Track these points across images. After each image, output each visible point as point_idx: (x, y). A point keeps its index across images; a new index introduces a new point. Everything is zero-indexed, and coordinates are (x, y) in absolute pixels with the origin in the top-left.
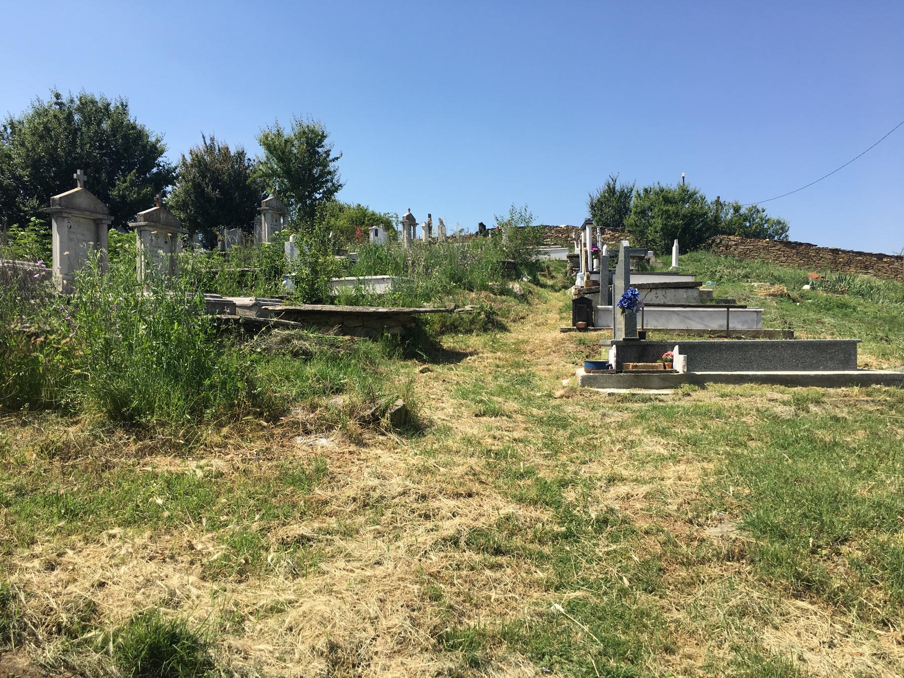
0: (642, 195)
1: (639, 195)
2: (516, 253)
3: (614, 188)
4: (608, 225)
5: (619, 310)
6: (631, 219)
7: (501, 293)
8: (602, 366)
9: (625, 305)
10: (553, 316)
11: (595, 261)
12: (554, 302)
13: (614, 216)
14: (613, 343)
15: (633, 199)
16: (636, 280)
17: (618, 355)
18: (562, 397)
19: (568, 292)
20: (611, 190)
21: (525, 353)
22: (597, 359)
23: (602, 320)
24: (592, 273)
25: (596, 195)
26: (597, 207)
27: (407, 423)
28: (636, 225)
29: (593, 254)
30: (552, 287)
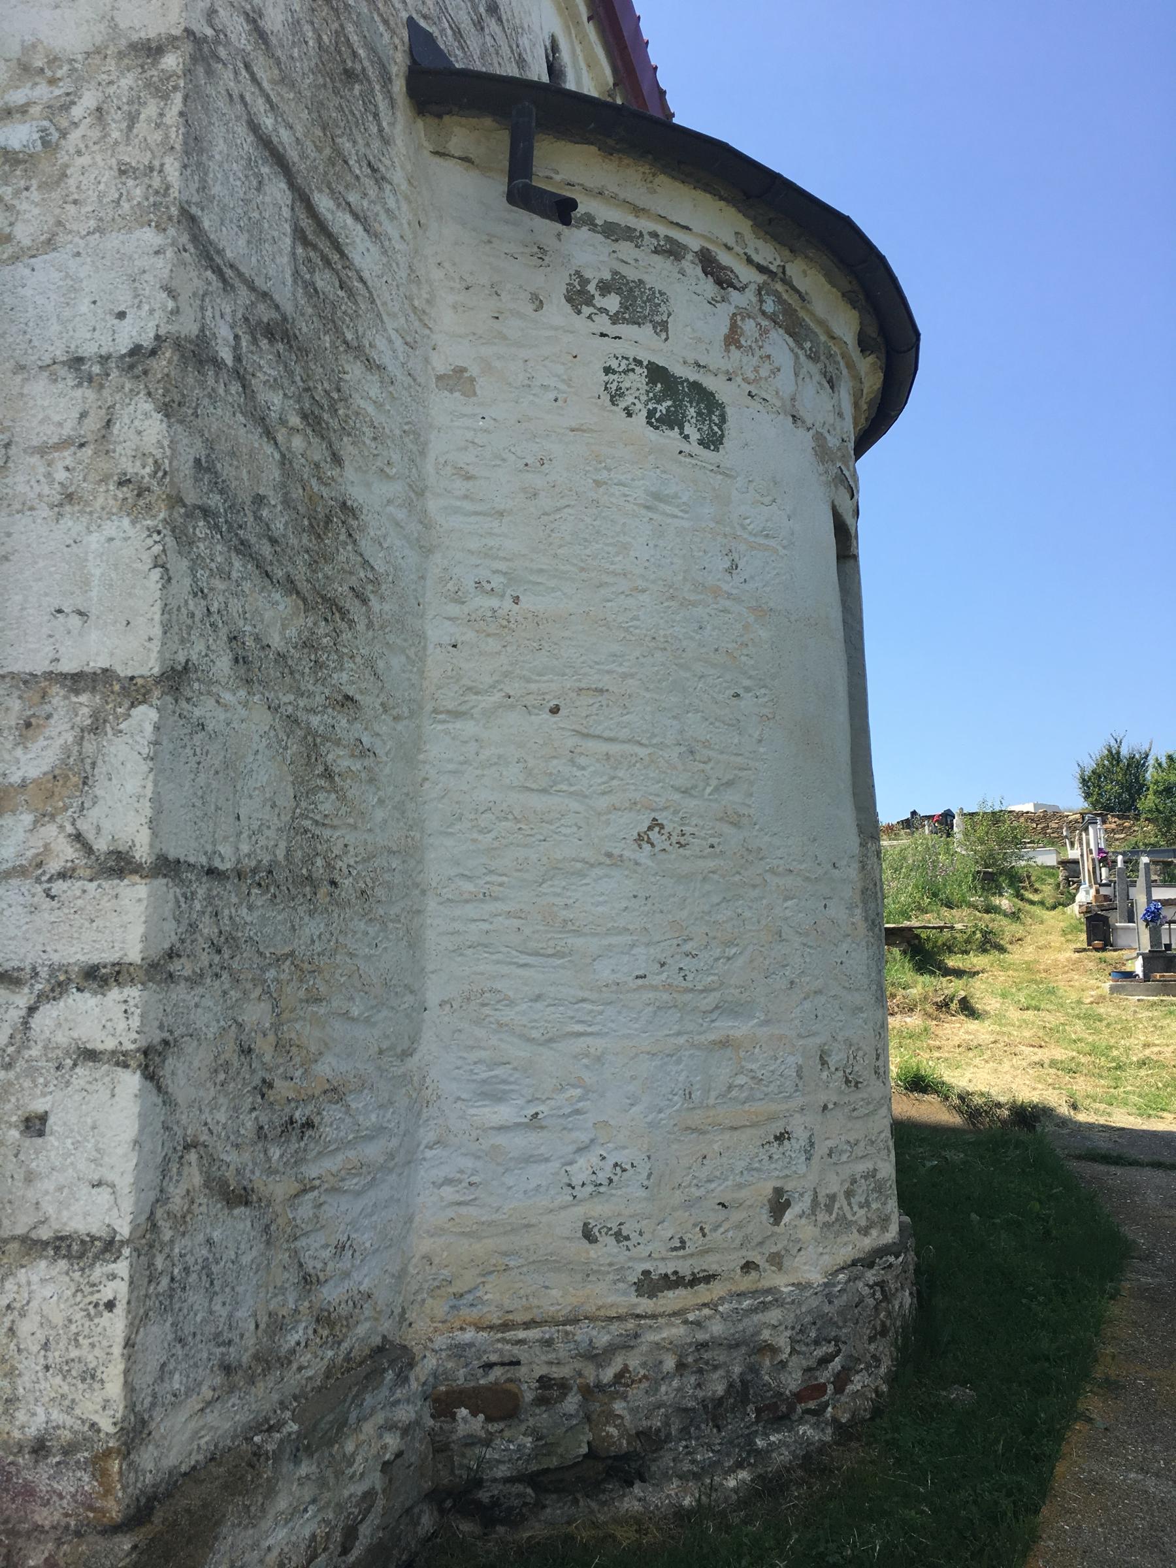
0: (1165, 765)
1: (1160, 765)
2: (989, 859)
3: (1118, 753)
4: (1111, 810)
5: (1142, 925)
6: (1148, 801)
7: (987, 911)
8: (1130, 975)
9: (1149, 918)
10: (1056, 939)
11: (1103, 869)
12: (1052, 922)
13: (1120, 795)
14: (1138, 955)
15: (1151, 770)
16: (1160, 894)
17: (1144, 966)
18: (1092, 1003)
19: (1068, 910)
20: (1114, 757)
21: (1039, 971)
22: (1123, 969)
23: (1121, 940)
24: (1101, 885)
25: (1090, 765)
26: (1091, 783)
27: (967, 1009)
28: (1158, 810)
29: (1100, 862)
30: (1042, 903)
